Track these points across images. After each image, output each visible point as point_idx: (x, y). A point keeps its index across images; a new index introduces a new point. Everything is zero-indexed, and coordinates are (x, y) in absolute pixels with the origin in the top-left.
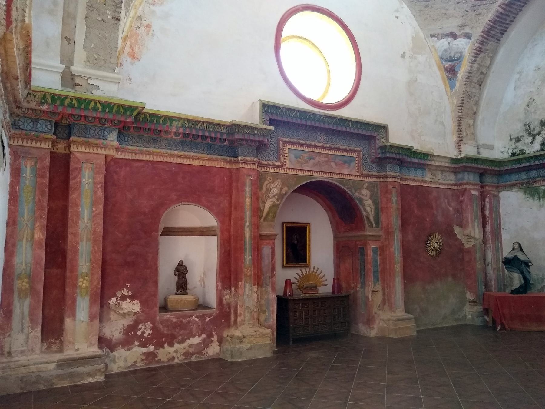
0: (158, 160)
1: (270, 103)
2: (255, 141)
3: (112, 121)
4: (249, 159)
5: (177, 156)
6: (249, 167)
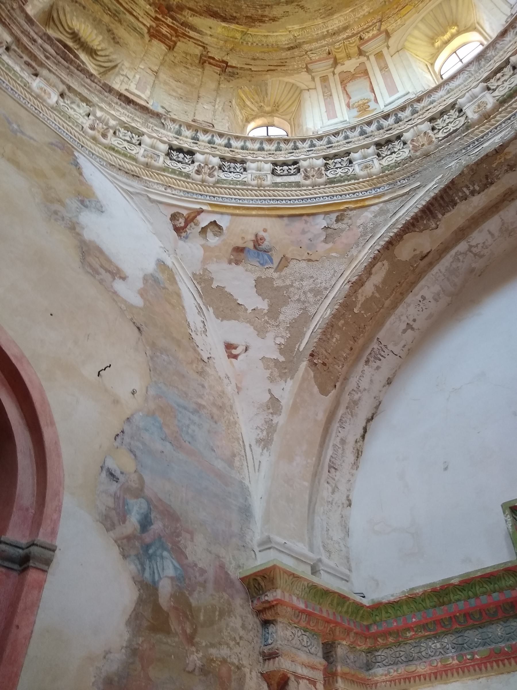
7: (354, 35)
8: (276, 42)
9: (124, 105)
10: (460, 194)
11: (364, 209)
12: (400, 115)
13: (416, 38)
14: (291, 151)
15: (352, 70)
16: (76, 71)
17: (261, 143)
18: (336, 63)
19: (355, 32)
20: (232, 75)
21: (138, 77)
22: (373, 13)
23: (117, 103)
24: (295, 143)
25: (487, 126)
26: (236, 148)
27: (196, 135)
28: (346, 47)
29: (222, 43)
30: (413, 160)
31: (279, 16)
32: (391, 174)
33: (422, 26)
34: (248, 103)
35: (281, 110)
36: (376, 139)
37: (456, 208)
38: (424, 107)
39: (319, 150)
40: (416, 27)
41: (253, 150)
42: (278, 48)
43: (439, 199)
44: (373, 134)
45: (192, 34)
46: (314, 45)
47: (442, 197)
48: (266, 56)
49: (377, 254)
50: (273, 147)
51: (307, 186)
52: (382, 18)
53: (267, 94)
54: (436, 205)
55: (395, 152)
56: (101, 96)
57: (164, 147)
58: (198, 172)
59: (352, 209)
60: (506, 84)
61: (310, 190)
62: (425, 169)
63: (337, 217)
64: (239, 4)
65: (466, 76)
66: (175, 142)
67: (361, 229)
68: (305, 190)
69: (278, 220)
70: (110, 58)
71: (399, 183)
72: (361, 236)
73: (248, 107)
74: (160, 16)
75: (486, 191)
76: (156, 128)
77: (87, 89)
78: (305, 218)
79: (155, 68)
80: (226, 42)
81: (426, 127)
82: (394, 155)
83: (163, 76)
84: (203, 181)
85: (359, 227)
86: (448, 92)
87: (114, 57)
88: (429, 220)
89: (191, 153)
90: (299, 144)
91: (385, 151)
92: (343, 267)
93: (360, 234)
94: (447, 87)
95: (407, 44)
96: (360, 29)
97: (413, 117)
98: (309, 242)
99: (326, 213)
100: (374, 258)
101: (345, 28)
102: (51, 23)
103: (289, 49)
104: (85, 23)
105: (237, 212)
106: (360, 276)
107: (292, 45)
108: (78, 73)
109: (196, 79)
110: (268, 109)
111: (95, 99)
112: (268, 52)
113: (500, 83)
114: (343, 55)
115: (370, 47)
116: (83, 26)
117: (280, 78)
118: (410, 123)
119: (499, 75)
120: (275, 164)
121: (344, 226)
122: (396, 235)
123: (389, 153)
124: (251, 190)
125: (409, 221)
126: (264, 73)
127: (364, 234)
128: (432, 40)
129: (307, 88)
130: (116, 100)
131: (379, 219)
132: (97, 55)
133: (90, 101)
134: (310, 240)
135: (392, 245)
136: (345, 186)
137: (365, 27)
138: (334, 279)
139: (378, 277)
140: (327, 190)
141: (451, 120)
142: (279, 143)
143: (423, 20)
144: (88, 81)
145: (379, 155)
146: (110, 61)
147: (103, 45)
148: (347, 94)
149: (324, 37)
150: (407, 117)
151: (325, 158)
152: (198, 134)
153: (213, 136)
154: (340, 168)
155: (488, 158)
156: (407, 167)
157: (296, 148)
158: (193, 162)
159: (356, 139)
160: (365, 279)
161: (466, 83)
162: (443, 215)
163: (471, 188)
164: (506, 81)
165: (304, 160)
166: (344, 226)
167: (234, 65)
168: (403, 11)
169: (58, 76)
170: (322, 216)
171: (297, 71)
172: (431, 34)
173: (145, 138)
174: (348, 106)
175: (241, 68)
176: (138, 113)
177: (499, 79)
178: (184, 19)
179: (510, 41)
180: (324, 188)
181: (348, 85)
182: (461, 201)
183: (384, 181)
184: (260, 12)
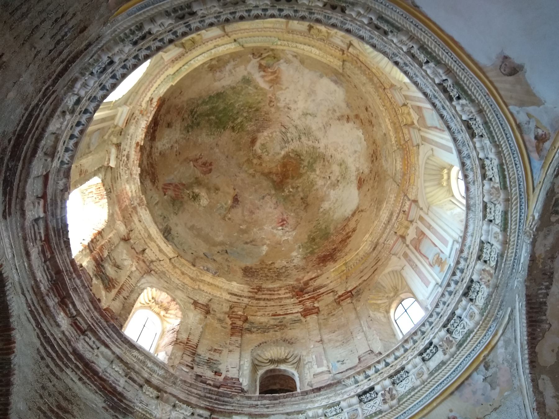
7: (399, 214)
8: (364, 252)
9: (318, 394)
10: (541, 296)
11: (495, 349)
12: (460, 266)
13: (431, 192)
14: (422, 337)
15: (415, 236)
16: (284, 400)
17: (403, 347)
18: (403, 237)
19: (398, 211)
20: (359, 293)
21: (314, 357)
22: (397, 195)
23: (314, 397)
24: (420, 330)
25: (511, 248)
26: (393, 362)
27: (366, 374)
28: (401, 224)
29: (339, 280)
30: (492, 295)
31: (355, 226)
32: (488, 313)
33: (427, 184)
34: (379, 302)
35: (399, 288)
36: (461, 292)
37: (548, 304)
38: (468, 253)
39: (436, 324)
40: (425, 187)
41: (402, 355)
42: (368, 255)
43: (531, 310)
44: (456, 289)
45: (322, 290)
46: (384, 236)
47: (531, 308)
48: (366, 265)
49: (531, 377)
50: (411, 343)
51: (449, 359)
52: (404, 193)
53: (384, 287)
54: (534, 315)
55: (478, 291)
56: (305, 401)
57: (355, 400)
58: (385, 401)
59: (488, 355)
60: (497, 212)
61: (453, 361)
62: (505, 296)
63: (484, 366)
64: (332, 239)
65: (472, 221)
66: (359, 391)
67: (506, 364)
68: (450, 363)
69: (452, 397)
70: (295, 355)
71: (499, 316)
72: (511, 368)
73: (381, 304)
74: (300, 299)
75: (554, 280)
76: (343, 391)
77: (295, 404)
78: (466, 383)
79: (319, 339)
80: (340, 277)
81: (480, 266)
82: (480, 294)
83: (326, 337)
84: (391, 407)
85: (503, 363)
86: (472, 236)
87: (296, 352)
88: (540, 326)
89: (372, 389)
90: (423, 329)
91: (472, 295)
92: (520, 399)
93: (508, 368)
94: (469, 234)
95: (429, 200)
96: (399, 208)
97: (468, 263)
98: (483, 397)
99: (476, 369)
100: (533, 381)
101: (392, 214)
102: (258, 368)
103: (374, 249)
104: (271, 349)
105: (425, 412)
106: (536, 401)
107: (373, 247)
108: (287, 399)
109: (343, 318)
110: (392, 295)
111: (303, 407)
112: (365, 261)
113: (493, 214)
114: (403, 229)
115: (413, 215)
116: (272, 352)
117: (383, 273)
118: (469, 267)
119: (488, 210)
120: (421, 354)
121: (494, 369)
122: (530, 354)
123: (476, 294)
124: (421, 390)
125: (528, 339)
126: (373, 275)
127: (511, 366)
128: (440, 184)
129: (401, 268)
130: (313, 395)
131: (510, 349)
132: (287, 359)
133: (302, 411)
134: (483, 395)
135: (535, 362)
136: (470, 341)
137: (400, 205)
138: (523, 411)
139: (549, 391)
140: (463, 353)
141: (490, 250)
142: (412, 338)
143: (425, 181)
144: (293, 399)
145: (471, 300)
146: (296, 357)
147: (287, 351)
148: (424, 256)
149: (385, 228)
150: (465, 265)
151: (444, 326)
152: (367, 373)
153: (375, 367)
154: (458, 325)
155: (531, 269)
156: (493, 303)
157: (423, 333)
158: (377, 394)
159: (450, 300)
160: (542, 399)
161: (476, 225)
162: (545, 315)
163: (543, 287)
164: (495, 211)
165: (434, 337)
166: (494, 369)
167: (355, 286)
168: (412, 181)
169: (279, 414)
170: (475, 373)
171: (388, 259)
172: (436, 183)
173: (343, 404)
174: (431, 265)
175: (360, 284)
176: (328, 391)
177: (490, 212)
178: (312, 287)
179: (475, 190)
180: (460, 353)
181: (421, 248)
182: (546, 298)
183: (489, 321)
184: (344, 233)
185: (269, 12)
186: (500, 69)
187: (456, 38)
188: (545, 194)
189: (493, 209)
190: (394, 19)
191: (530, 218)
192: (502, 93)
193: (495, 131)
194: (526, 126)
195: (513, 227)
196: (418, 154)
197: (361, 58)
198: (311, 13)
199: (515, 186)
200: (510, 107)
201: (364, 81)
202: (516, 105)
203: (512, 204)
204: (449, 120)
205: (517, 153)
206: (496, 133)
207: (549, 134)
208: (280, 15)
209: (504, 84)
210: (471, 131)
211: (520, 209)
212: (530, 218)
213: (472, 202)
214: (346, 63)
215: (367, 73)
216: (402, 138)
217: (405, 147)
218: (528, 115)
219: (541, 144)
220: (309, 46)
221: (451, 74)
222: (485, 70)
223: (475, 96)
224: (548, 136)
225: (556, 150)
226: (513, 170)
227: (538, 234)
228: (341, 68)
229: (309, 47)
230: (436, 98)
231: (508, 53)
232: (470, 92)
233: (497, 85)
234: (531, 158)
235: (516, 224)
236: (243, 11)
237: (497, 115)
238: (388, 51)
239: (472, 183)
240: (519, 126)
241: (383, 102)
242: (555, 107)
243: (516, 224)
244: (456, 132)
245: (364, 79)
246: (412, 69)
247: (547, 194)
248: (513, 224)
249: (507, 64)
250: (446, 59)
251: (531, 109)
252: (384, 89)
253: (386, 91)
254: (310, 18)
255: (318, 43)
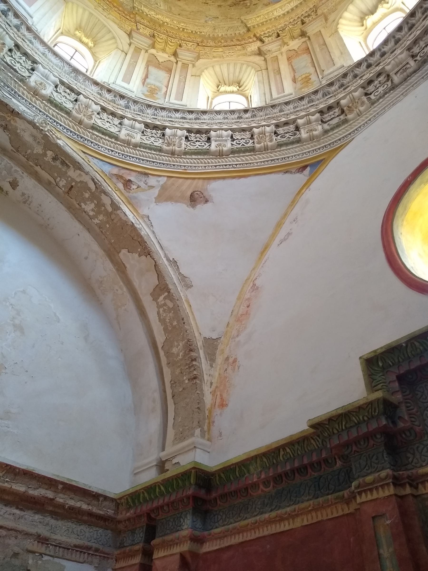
0: (249, 538)
1: (379, 351)
2: (367, 437)
3: (182, 500)
4: (369, 479)
5: (270, 522)
6: (375, 495)
13: (77, 12)
33: (87, 13)
40: (84, 10)
60: (64, 99)
86: (43, 54)
95: (70, 5)
113: (63, 94)
119: (68, 91)
128: (79, 28)
164: (66, 98)
172: (83, 24)
185: (378, 55)
186: (200, 192)
187: (242, 180)
188: (80, 162)
189: (68, 97)
190: (289, 149)
191: (58, 135)
192: (181, 180)
193: (151, 153)
194: (144, 180)
195: (51, 111)
196: (121, 28)
197: (239, 47)
198: (342, 85)
199: (91, 138)
200: (166, 178)
201: (217, 31)
202: (165, 183)
203: (75, 125)
204: (170, 114)
205: (123, 159)
206: (147, 153)
207: (129, 192)
208: (366, 61)
209: (188, 187)
210: (151, 126)
211: (67, 129)
212: (58, 135)
213: (80, 78)
214: (245, 30)
215: (223, 41)
216: (142, 21)
217: (132, 16)
218: (152, 187)
219: (123, 181)
220: (288, 12)
221: (218, 154)
222: (206, 181)
223: (188, 159)
224: (128, 190)
225: (114, 190)
226: (107, 145)
227: (42, 134)
228: (245, 21)
229: (287, 10)
230: (196, 119)
231: (209, 204)
232: (194, 157)
233: (189, 181)
234: (114, 167)
235: (53, 116)
236: (403, 37)
237: (164, 164)
238: (261, 114)
239: (100, 92)
240: (146, 174)
241: (187, 33)
242: (149, 208)
243: (53, 116)
244: (156, 112)
245: (220, 33)
246: (233, 119)
247: (78, 163)
248: (54, 113)
249: (201, 199)
250: (232, 160)
251: (156, 192)
252: (198, 44)
253: (196, 44)
254: (339, 81)
255: (282, 23)
